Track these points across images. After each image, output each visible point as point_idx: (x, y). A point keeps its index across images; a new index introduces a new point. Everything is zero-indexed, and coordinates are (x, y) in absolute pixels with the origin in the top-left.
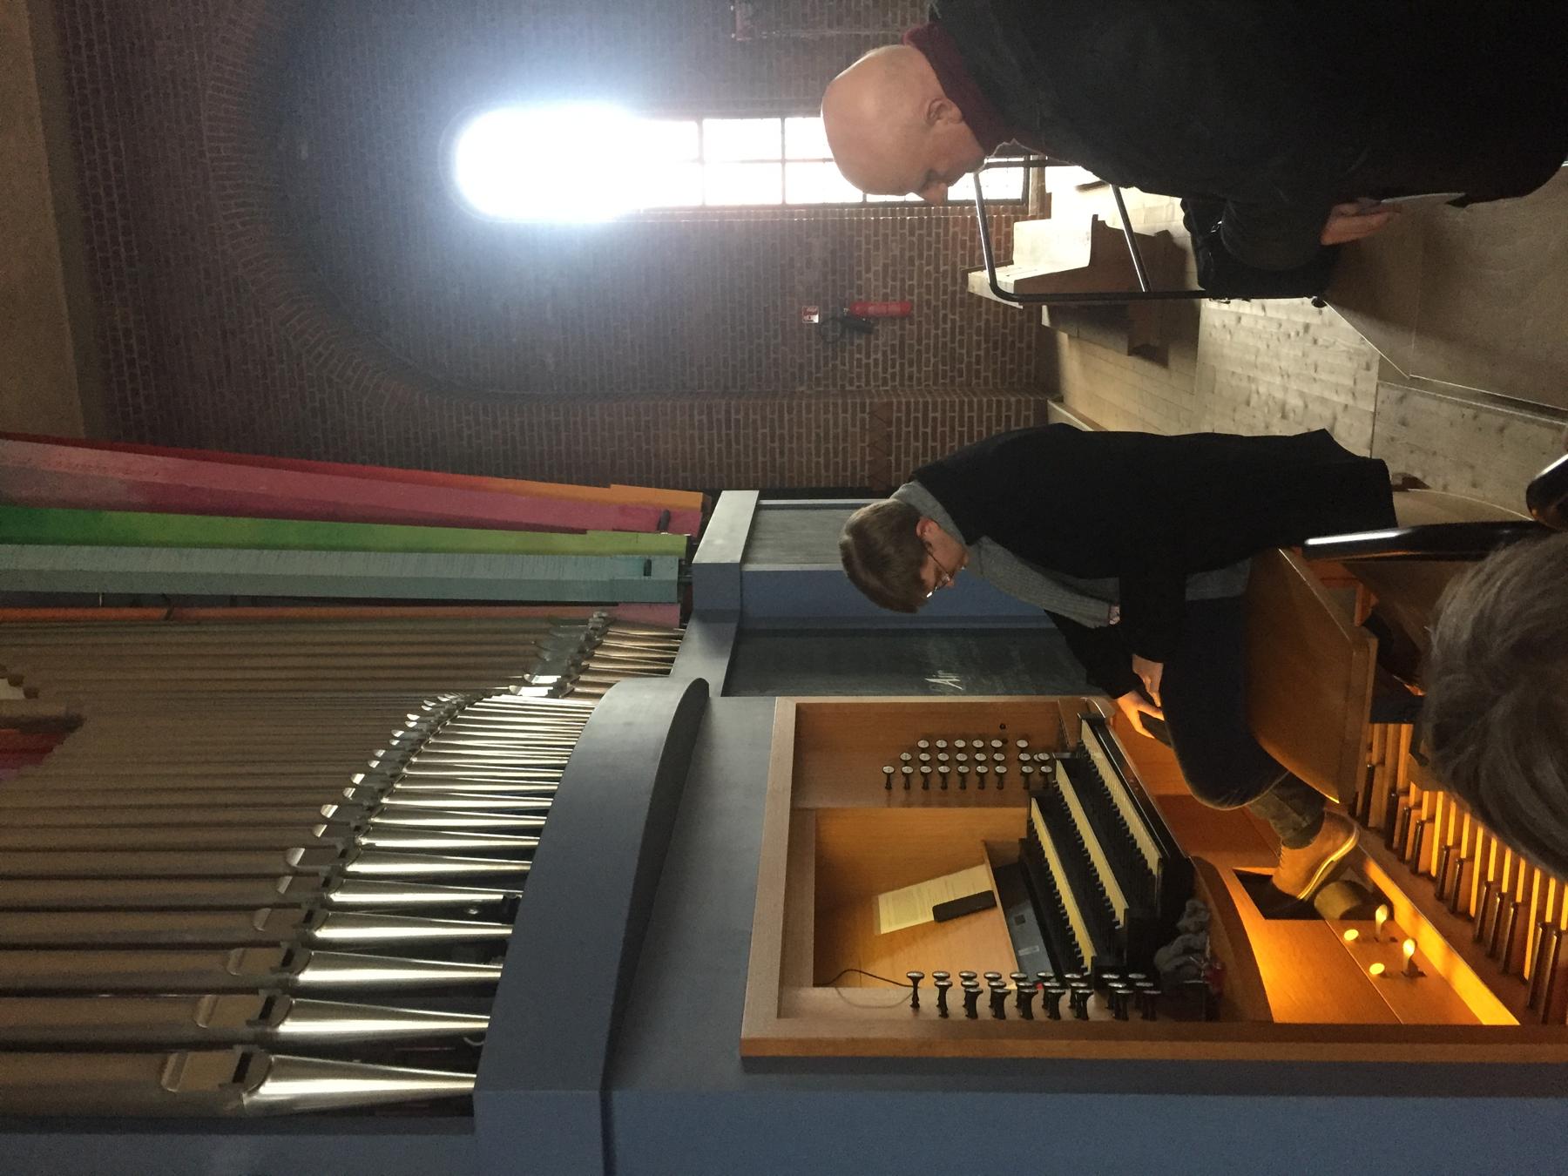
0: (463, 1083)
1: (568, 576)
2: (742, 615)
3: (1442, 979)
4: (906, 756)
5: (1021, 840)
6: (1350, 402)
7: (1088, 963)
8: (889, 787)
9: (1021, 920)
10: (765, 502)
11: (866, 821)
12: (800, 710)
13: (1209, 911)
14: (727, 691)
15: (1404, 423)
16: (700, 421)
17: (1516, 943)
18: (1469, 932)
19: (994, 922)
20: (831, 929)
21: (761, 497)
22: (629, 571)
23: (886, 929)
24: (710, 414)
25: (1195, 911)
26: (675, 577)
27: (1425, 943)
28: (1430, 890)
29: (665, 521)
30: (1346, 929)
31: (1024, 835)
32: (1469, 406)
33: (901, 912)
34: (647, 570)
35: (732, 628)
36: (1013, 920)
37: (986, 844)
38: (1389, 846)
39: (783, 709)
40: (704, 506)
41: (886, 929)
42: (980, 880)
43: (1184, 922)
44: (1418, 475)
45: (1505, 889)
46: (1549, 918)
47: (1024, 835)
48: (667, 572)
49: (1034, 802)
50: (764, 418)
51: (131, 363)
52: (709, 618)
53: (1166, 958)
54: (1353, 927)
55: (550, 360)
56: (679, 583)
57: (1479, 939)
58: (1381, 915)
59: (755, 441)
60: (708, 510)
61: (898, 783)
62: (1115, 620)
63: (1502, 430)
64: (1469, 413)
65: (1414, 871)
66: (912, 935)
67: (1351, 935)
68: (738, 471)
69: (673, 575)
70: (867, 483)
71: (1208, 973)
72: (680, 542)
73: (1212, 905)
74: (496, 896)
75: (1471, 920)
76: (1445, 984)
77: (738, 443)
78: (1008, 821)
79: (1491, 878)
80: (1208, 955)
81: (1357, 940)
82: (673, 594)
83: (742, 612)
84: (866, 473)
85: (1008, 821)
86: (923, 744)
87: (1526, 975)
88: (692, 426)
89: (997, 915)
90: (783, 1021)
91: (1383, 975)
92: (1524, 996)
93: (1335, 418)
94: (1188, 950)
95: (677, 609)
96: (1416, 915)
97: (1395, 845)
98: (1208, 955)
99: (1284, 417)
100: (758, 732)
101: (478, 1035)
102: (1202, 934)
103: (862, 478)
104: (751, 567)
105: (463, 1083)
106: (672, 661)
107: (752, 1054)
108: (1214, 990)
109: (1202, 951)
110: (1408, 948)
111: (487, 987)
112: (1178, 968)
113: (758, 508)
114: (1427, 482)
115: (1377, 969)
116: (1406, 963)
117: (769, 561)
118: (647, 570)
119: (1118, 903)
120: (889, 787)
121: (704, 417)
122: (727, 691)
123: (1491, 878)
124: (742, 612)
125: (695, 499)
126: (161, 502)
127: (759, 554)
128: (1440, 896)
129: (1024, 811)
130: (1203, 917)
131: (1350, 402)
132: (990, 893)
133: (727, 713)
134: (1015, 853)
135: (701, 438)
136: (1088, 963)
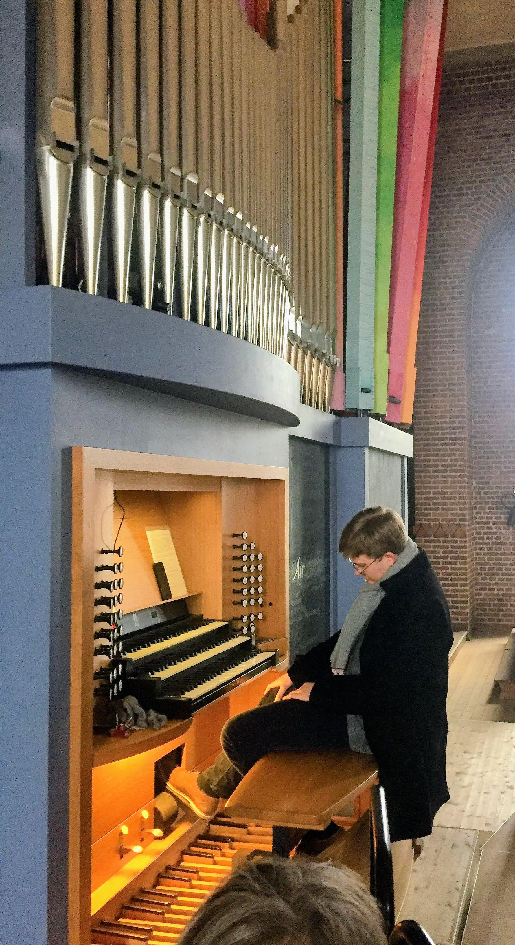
1: (361, 342)
7: (128, 655)
8: (235, 536)
9: (154, 615)
11: (215, 522)
12: (280, 482)
13: (160, 729)
14: (292, 438)
18: (147, 886)
20: (152, 501)
21: (409, 459)
22: (364, 380)
24: (459, 428)
25: (160, 720)
28: (172, 862)
30: (149, 811)
31: (205, 617)
33: (160, 542)
34: (364, 390)
35: (330, 441)
36: (154, 610)
37: (200, 594)
38: (199, 837)
40: (403, 424)
43: (153, 713)
44: (422, 854)
47: (205, 617)
48: (364, 402)
50: (456, 460)
51: (490, 79)
52: (336, 425)
53: (131, 703)
54: (150, 815)
55: (491, 331)
56: (357, 409)
57: (143, 892)
58: (158, 832)
59: (443, 455)
60: (401, 426)
64: (460, 885)
65: (183, 853)
66: (146, 550)
69: (362, 406)
71: (122, 728)
72: (382, 409)
75: (154, 887)
79: (180, 898)
80: (134, 728)
81: (142, 818)
82: (351, 406)
83: (339, 447)
86: (260, 556)
91: (121, 834)
92: (108, 918)
93: (456, 805)
94: (136, 716)
95: (342, 408)
97: (200, 841)
99: (457, 774)
100: (267, 455)
102: (145, 725)
104: (367, 451)
106: (310, 405)
108: (112, 731)
109: (135, 724)
110: (137, 849)
112: (125, 710)
113: (402, 457)
115: (125, 830)
116: (126, 847)
117: (370, 463)
118: (364, 390)
119: (164, 674)
120: (235, 536)
121: (457, 425)
122: (292, 438)
124: (339, 447)
125: (408, 419)
127: (375, 456)
128: (168, 868)
129: (220, 618)
131: (466, 814)
132: (170, 597)
134: (195, 612)
135: (444, 423)
136: (128, 655)
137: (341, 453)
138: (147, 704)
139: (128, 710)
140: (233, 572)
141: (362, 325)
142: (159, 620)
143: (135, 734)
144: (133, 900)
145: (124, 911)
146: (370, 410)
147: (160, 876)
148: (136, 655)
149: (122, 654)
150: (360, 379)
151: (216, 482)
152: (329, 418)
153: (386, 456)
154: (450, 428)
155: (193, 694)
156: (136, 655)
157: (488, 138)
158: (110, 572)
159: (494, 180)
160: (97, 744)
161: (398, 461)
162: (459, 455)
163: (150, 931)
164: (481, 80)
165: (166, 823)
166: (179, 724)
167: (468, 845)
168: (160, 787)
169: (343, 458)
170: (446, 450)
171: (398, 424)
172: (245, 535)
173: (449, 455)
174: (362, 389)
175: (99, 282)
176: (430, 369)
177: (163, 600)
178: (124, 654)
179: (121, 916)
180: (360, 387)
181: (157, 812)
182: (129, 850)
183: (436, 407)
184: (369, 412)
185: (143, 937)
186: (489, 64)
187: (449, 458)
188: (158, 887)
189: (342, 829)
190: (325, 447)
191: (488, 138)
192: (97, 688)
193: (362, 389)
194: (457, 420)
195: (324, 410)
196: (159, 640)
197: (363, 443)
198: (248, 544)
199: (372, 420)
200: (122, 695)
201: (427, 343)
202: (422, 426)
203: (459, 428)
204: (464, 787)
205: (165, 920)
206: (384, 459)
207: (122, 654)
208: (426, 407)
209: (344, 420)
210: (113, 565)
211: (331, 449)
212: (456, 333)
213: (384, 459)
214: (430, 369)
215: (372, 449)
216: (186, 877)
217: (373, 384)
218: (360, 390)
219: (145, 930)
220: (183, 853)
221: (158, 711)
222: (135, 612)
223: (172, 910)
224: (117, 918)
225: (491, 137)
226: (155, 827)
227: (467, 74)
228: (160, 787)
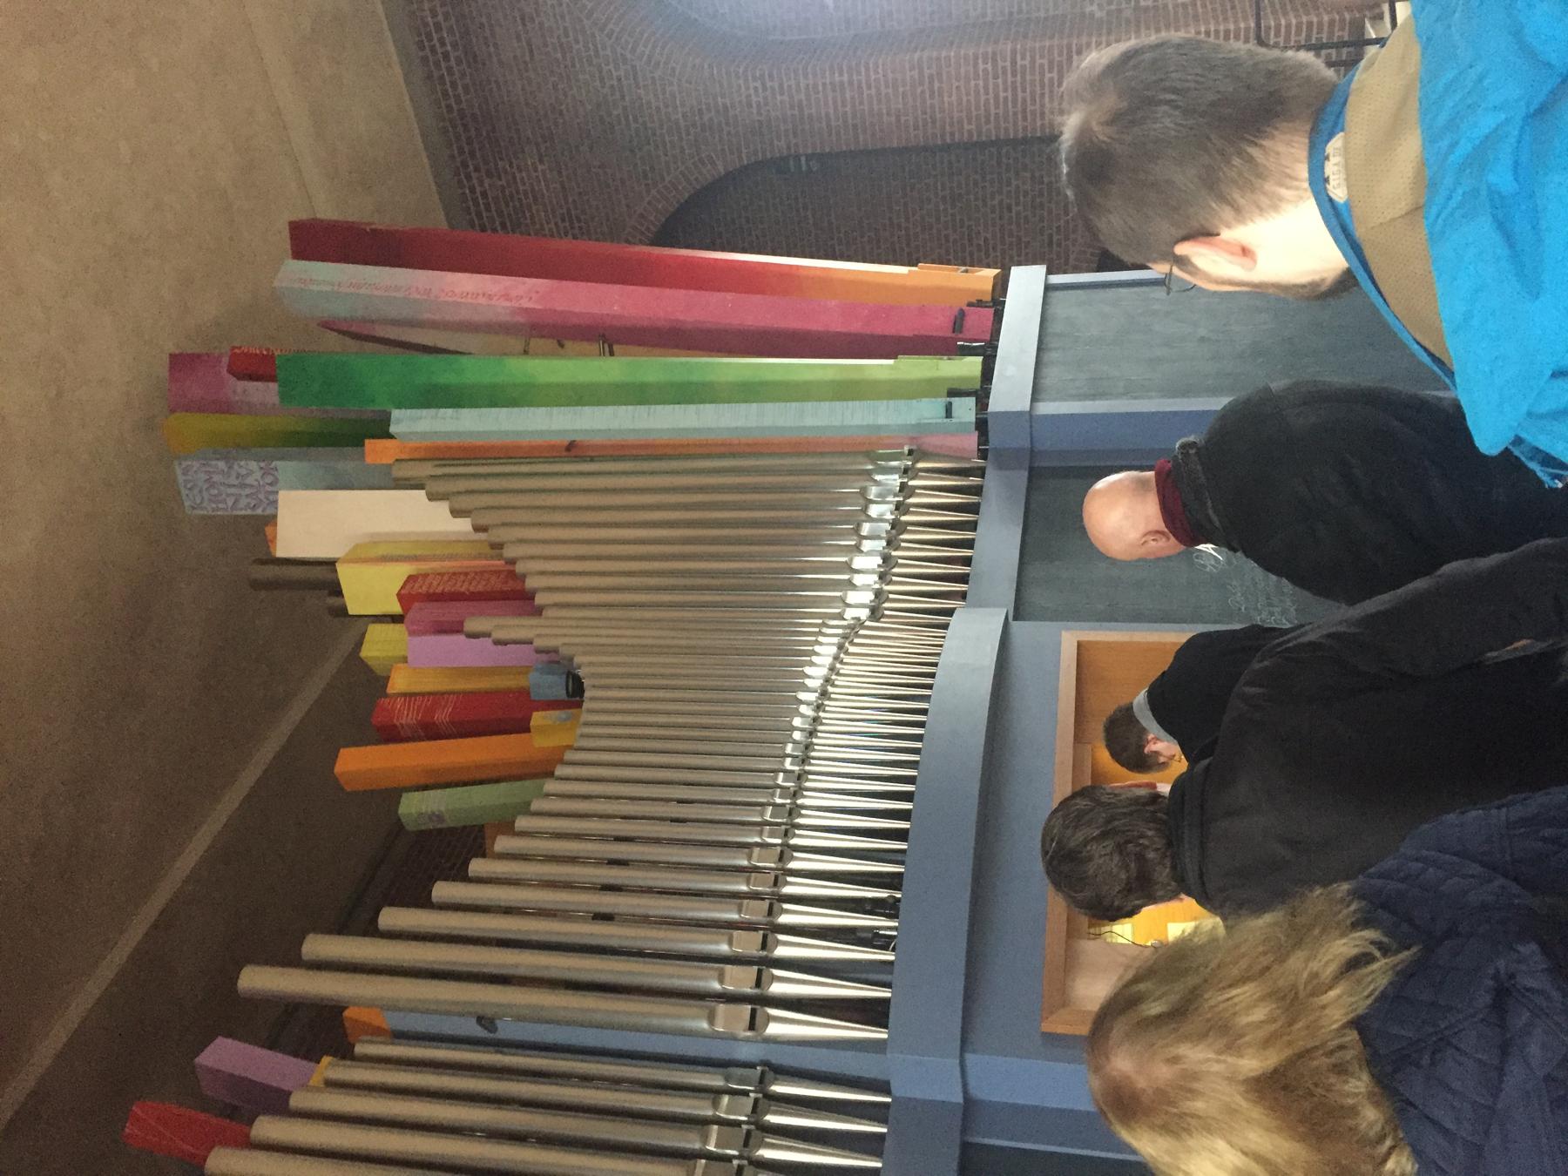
0: (903, 846)
1: (881, 421)
10: (1057, 279)
16: (985, 70)
21: (1049, 272)
22: (928, 410)
24: (994, 60)
39: (1069, 639)
48: (965, 409)
50: (1051, 63)
51: (446, 56)
52: (1005, 460)
59: (1043, 87)
60: (1001, 285)
62: (1533, 947)
68: (1025, 119)
72: (973, 365)
74: (882, 894)
77: (1024, 91)
83: (1032, 450)
88: (977, 77)
101: (884, 1041)
105: (903, 846)
111: (903, 851)
113: (1048, 288)
121: (989, 66)
124: (1032, 450)
125: (986, 276)
126: (558, 333)
135: (986, 88)
137: (1038, 447)
141: (857, 421)
154: (996, 77)
157: (531, 51)
159: (593, 35)
162: (1042, 57)
164: (449, 69)
170: (1033, 82)
173: (1042, 74)
175: (845, 910)
176: (898, 120)
183: (960, 104)
186: (425, 60)
187: (1048, 75)
190: (1034, 475)
191: (531, 51)
194: (981, 66)
201: (855, 126)
202: (992, 126)
203: (994, 60)
208: (960, 122)
212: (837, 78)
214: (898, 120)
215: (1036, 396)
225: (529, 44)
227: (445, 94)
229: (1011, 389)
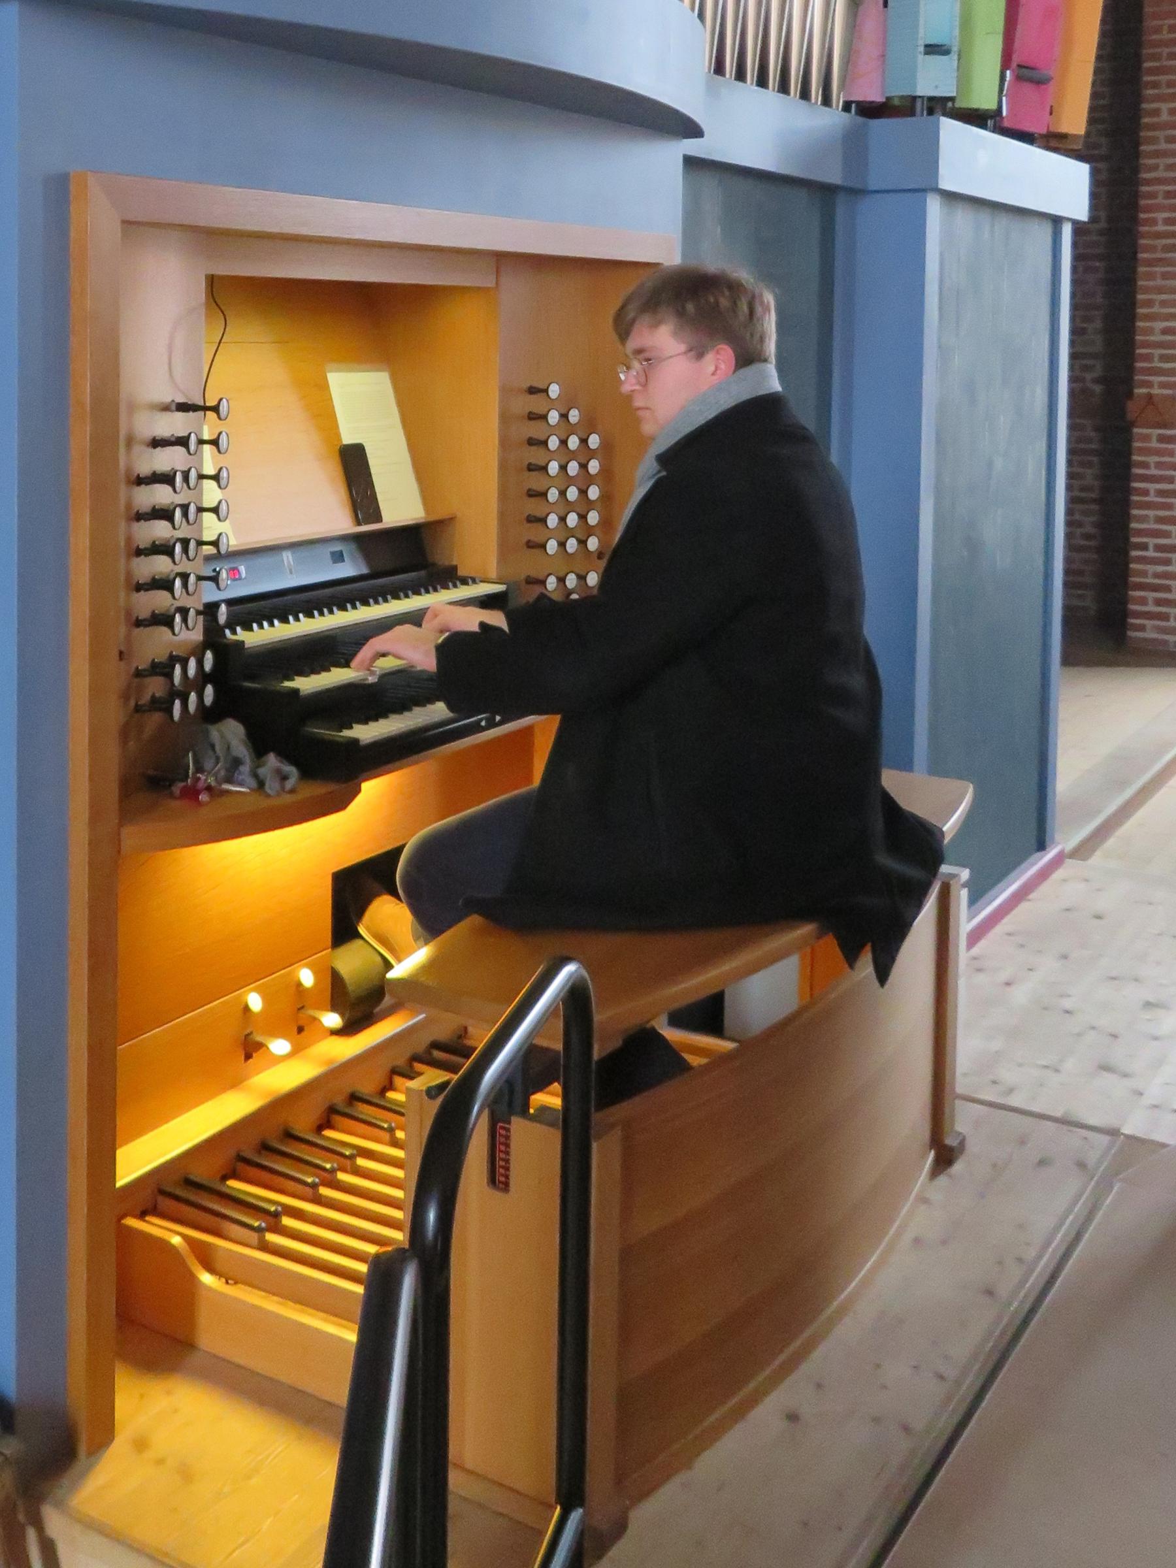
2: (856, 193)
3: (242, 1082)
4: (574, 416)
5: (455, 568)
6: (1147, 1100)
7: (241, 635)
8: (532, 391)
9: (338, 557)
10: (1067, 231)
11: (478, 355)
13: (278, 795)
14: (691, 163)
15: (1042, 1163)
17: (265, 1176)
18: (302, 1124)
19: (334, 517)
21: (1075, 223)
23: (780, 389)
25: (284, 778)
26: (919, 94)
27: (285, 1069)
28: (367, 1088)
29: (1025, 71)
30: (315, 973)
31: (461, 572)
32: (1039, 1257)
33: (362, 401)
34: (933, 49)
35: (833, 175)
36: (338, 547)
37: (452, 519)
38: (435, 1045)
40: (1063, 137)
41: (780, 389)
42: (400, 504)
43: (272, 760)
44: (958, 1167)
45: (342, 1176)
46: (287, 1221)
47: (461, 572)
48: (933, 79)
49: (500, 588)
52: (853, 148)
53: (231, 734)
54: (317, 984)
56: (914, 99)
57: (289, 1136)
58: (332, 1020)
60: (1054, 142)
61: (536, 404)
63: (990, 1293)
64: (1031, 1253)
65: (395, 1072)
66: (323, 415)
67: (307, 977)
69: (925, 88)
70: (1140, 391)
71: (201, 785)
73: (288, 799)
75: (319, 1129)
76: (235, 1083)
78: (480, 550)
79: (361, 1162)
80: (226, 786)
81: (299, 984)
82: (897, 91)
84: (1156, 391)
85: (480, 550)
86: (594, 441)
87: (232, 1183)
89: (341, 522)
90: (118, 226)
91: (246, 1009)
92: (199, 1173)
93: (1126, 1075)
94: (237, 762)
95: (876, 96)
96: (331, 1061)
97: (437, 1054)
98: (226, 786)
99: (1148, 1005)
102: (253, 783)
103: (1149, 385)
104: (934, 207)
106: (762, 82)
107: (72, 188)
108: (177, 788)
109: (229, 780)
110: (279, 1046)
112: (213, 747)
114: (942, 1180)
115: (255, 1002)
116: (259, 1038)
117: (948, 236)
118: (933, 49)
119: (307, 684)
120: (532, 391)
122: (691, 163)
123: (361, 1162)
125: (1075, 119)
127: (963, 218)
128: (354, 1098)
129: (493, 575)
130: (272, 786)
131: (1147, 1100)
132: (379, 519)
133: (665, 158)
134: (442, 559)
136: (241, 635)
138: (261, 743)
139: (217, 748)
140: (527, 474)
142: (347, 570)
143: (225, 800)
144: (265, 1148)
145: (240, 1166)
146: (952, 99)
147: (332, 1110)
148: (256, 637)
149: (227, 632)
150: (922, 22)
151: (939, 339)
152: (833, 119)
153: (1003, 220)
155: (366, 733)
156: (256, 637)
158: (180, 450)
160: (128, 811)
161: (1044, 232)
163: (276, 1215)
165: (361, 1005)
166: (331, 787)
167: (1081, 1165)
168: (344, 929)
169: (870, 221)
171: (1042, 136)
172: (554, 391)
174: (926, 46)
177: (359, 524)
178: (234, 632)
179: (234, 1175)
180: (921, 43)
181: (336, 977)
182: (260, 1046)
184: (950, 104)
185: (256, 1224)
188: (328, 1133)
189: (685, 1067)
192: (157, 695)
193: (926, 46)
195: (827, 101)
196: (325, 610)
197: (924, 183)
198: (563, 412)
199: (949, 127)
200: (210, 715)
204: (1156, 1038)
205: (319, 1200)
206: (993, 226)
207: (227, 632)
209: (878, 126)
210: (186, 434)
211: (841, 201)
213: (993, 226)
215: (951, 197)
216: (386, 1121)
217: (957, 32)
218: (922, 49)
219: (266, 1212)
220: (395, 1072)
221: (286, 755)
222: (293, 546)
223: (339, 1181)
224: (224, 1178)
226: (334, 1008)
228: (344, 929)
229: (974, 160)
